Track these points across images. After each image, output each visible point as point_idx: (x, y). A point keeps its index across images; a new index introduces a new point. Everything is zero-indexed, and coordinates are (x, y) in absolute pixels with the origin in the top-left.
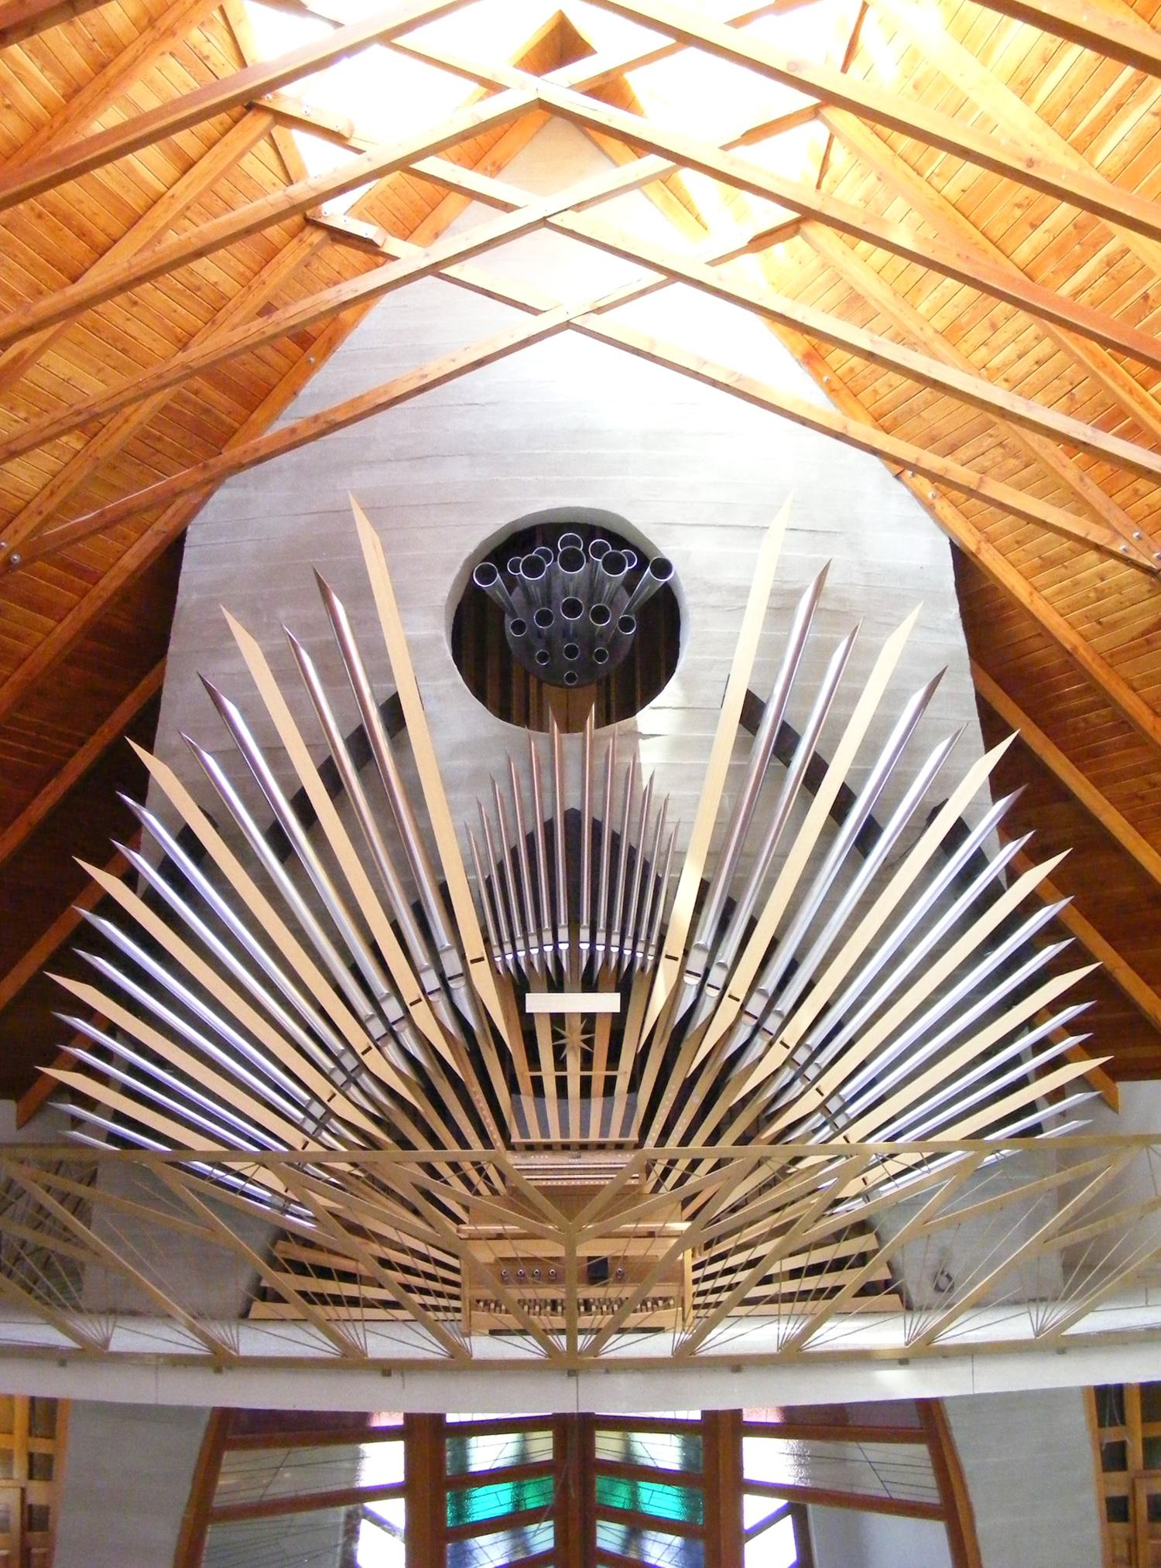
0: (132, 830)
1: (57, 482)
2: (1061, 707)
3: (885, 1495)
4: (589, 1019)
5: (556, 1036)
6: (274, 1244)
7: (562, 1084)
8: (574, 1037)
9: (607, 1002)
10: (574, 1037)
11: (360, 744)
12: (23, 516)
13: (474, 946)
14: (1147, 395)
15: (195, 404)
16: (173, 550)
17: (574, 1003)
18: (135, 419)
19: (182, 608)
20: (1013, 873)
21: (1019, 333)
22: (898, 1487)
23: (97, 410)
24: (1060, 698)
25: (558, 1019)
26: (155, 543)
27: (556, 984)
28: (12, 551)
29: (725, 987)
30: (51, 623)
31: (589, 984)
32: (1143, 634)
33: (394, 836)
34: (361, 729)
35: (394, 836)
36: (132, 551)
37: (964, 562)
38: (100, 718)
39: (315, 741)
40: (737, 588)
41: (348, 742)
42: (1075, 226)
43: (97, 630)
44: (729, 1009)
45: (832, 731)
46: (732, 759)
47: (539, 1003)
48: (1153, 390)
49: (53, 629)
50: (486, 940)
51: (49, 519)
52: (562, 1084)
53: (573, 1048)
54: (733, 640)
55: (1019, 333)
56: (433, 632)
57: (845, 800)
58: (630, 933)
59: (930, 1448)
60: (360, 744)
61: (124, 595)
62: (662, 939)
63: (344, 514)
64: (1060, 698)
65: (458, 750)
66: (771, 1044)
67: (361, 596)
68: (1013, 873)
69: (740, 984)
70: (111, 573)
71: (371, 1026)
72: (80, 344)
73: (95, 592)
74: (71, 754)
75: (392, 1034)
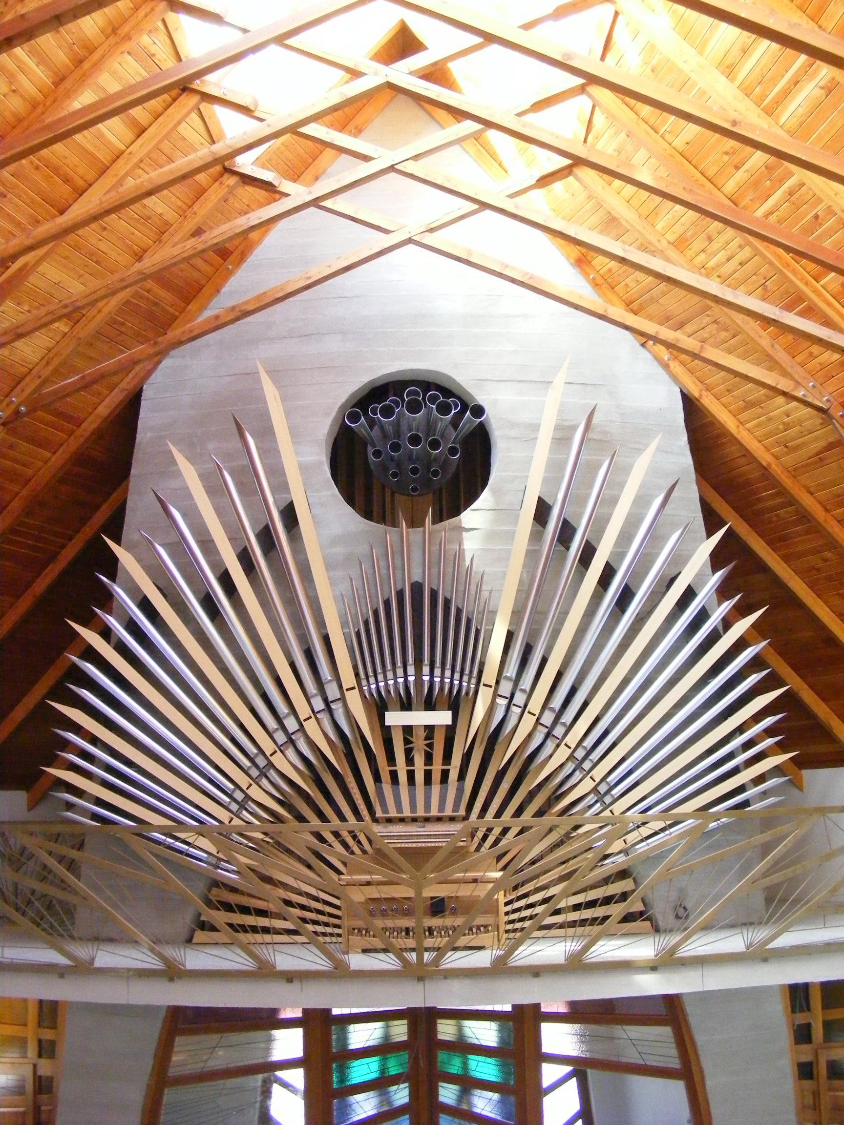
0: (107, 600)
1: (51, 355)
2: (760, 506)
3: (641, 1062)
4: (430, 729)
5: (407, 741)
6: (209, 890)
7: (411, 775)
8: (419, 742)
9: (443, 718)
10: (419, 742)
11: (267, 537)
12: (27, 379)
13: (348, 678)
14: (818, 286)
15: (148, 299)
16: (134, 401)
17: (419, 718)
18: (106, 310)
19: (140, 443)
20: (727, 623)
21: (728, 243)
22: (654, 1057)
23: (79, 304)
24: (759, 500)
25: (408, 730)
26: (121, 397)
27: (406, 705)
28: (20, 404)
29: (526, 706)
30: (48, 454)
31: (430, 705)
32: (817, 454)
33: (291, 602)
34: (267, 527)
35: (291, 602)
36: (104, 403)
37: (690, 405)
38: (84, 521)
39: (235, 534)
40: (530, 425)
41: (258, 536)
42: (766, 167)
43: (80, 459)
44: (528, 722)
45: (599, 524)
46: (528, 545)
47: (395, 718)
48: (822, 283)
49: (50, 459)
50: (357, 675)
51: (45, 382)
52: (411, 775)
53: (418, 750)
54: (529, 461)
55: (728, 243)
56: (317, 458)
57: (608, 573)
58: (458, 669)
59: (674, 1029)
60: (267, 537)
61: (99, 434)
62: (480, 672)
63: (254, 375)
64: (759, 500)
65: (336, 541)
66: (558, 746)
67: (266, 433)
68: (727, 623)
69: (535, 704)
70: (90, 419)
71: (276, 736)
72: (66, 258)
73: (79, 432)
74: (63, 547)
75: (291, 742)
